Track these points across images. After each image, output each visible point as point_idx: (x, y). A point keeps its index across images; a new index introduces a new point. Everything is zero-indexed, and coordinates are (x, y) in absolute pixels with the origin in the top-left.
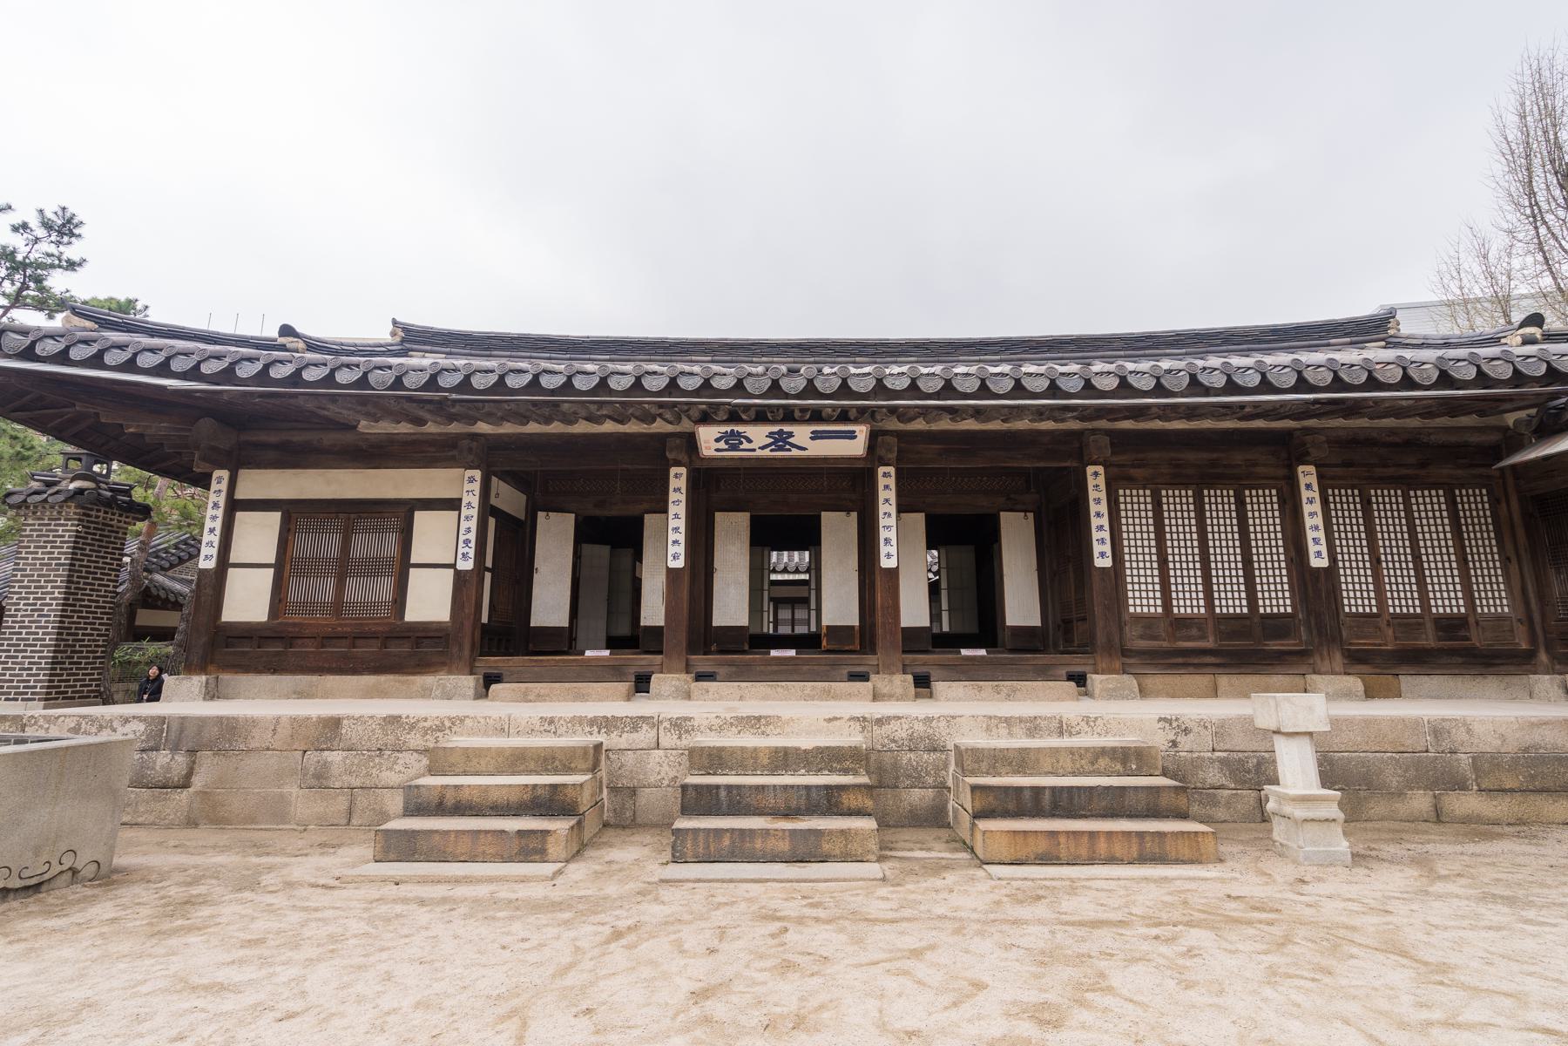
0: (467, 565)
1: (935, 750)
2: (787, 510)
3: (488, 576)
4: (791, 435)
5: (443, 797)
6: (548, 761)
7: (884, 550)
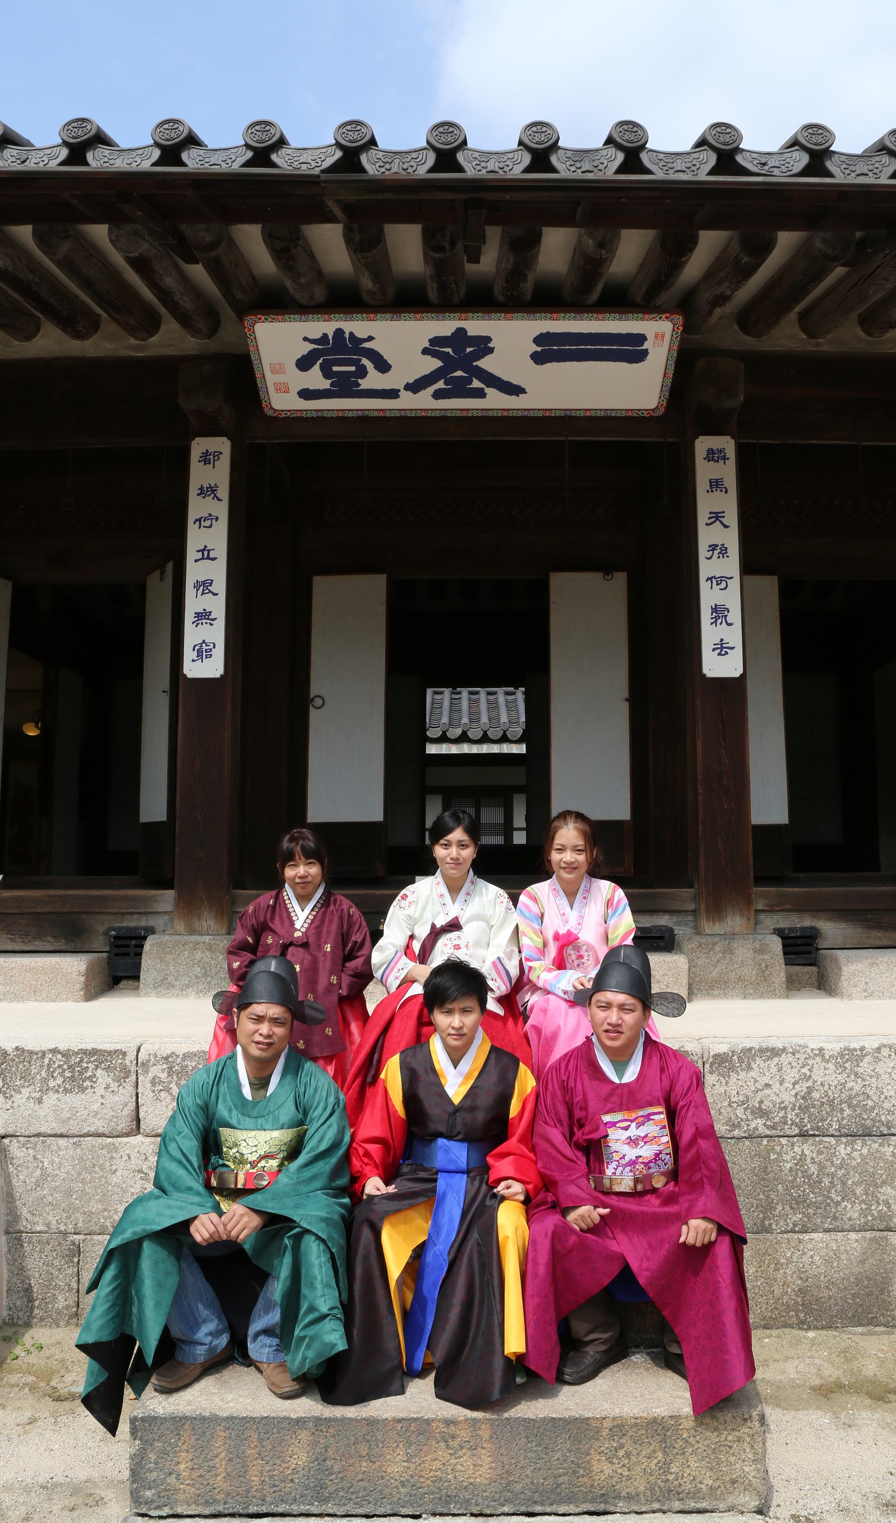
1: (867, 1134)
2: (468, 546)
4: (483, 346)
7: (710, 634)
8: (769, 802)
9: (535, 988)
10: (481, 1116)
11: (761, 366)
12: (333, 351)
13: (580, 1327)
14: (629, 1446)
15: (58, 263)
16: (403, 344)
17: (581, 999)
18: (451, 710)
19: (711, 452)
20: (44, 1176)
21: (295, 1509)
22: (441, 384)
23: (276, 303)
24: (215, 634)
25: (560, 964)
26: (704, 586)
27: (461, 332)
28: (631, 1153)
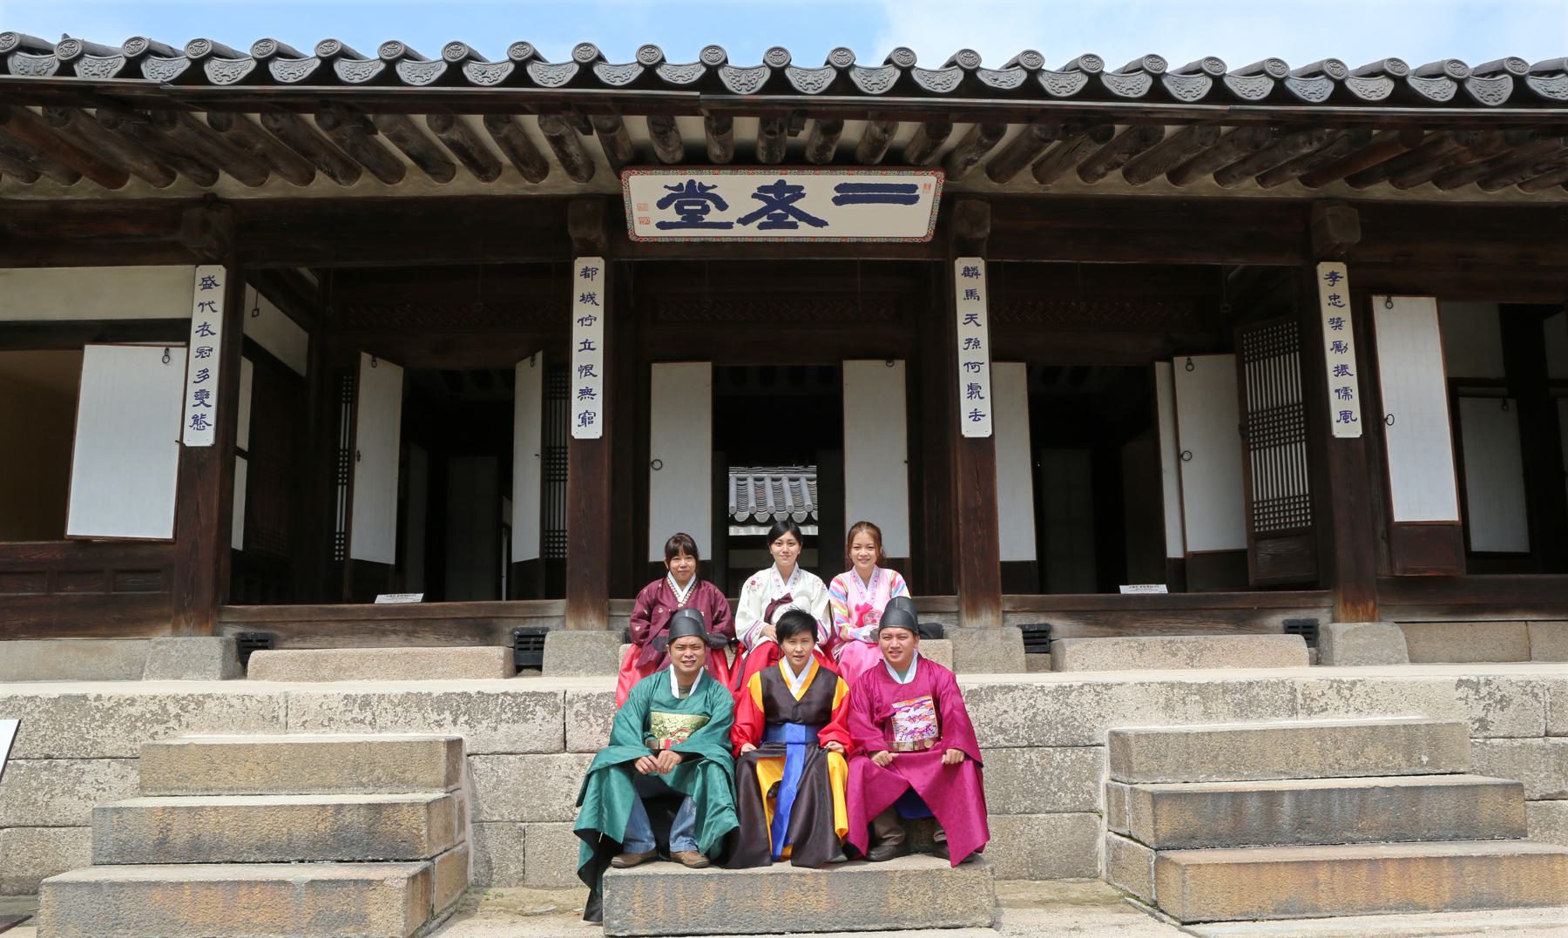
0: (204, 438)
3: (241, 466)
4: (798, 192)
5: (167, 828)
6: (359, 764)
7: (966, 405)
8: (1017, 540)
9: (843, 641)
10: (814, 708)
11: (1002, 204)
12: (687, 194)
13: (881, 829)
14: (911, 888)
15: (499, 141)
16: (738, 191)
17: (874, 641)
18: (738, 496)
19: (967, 269)
20: (499, 782)
21: (707, 930)
22: (764, 219)
23: (643, 160)
24: (596, 405)
25: (861, 624)
26: (962, 370)
27: (781, 183)
28: (911, 726)
